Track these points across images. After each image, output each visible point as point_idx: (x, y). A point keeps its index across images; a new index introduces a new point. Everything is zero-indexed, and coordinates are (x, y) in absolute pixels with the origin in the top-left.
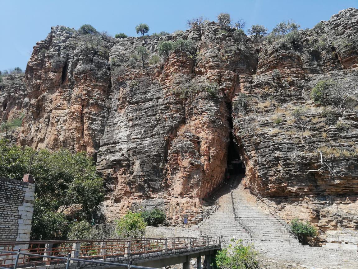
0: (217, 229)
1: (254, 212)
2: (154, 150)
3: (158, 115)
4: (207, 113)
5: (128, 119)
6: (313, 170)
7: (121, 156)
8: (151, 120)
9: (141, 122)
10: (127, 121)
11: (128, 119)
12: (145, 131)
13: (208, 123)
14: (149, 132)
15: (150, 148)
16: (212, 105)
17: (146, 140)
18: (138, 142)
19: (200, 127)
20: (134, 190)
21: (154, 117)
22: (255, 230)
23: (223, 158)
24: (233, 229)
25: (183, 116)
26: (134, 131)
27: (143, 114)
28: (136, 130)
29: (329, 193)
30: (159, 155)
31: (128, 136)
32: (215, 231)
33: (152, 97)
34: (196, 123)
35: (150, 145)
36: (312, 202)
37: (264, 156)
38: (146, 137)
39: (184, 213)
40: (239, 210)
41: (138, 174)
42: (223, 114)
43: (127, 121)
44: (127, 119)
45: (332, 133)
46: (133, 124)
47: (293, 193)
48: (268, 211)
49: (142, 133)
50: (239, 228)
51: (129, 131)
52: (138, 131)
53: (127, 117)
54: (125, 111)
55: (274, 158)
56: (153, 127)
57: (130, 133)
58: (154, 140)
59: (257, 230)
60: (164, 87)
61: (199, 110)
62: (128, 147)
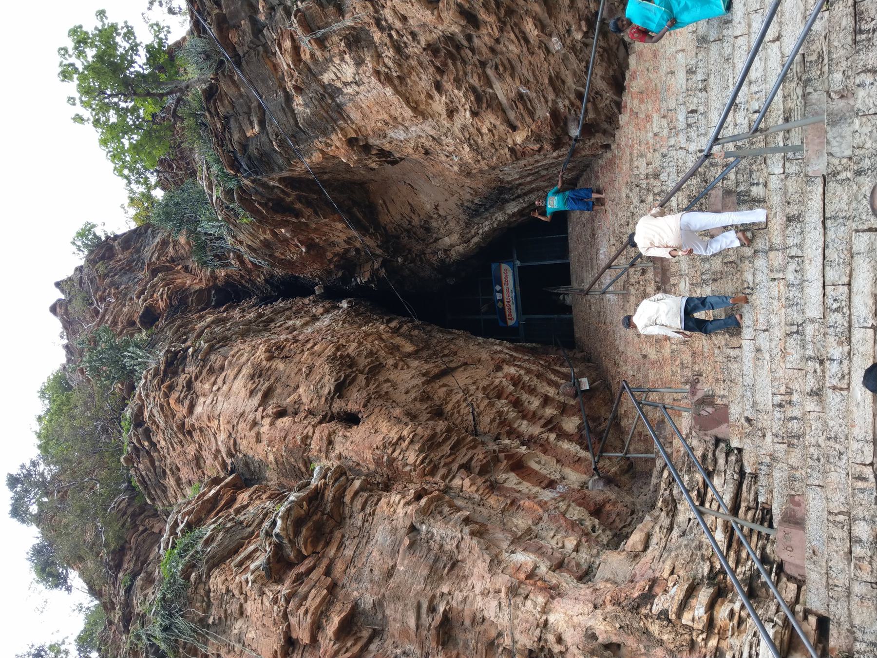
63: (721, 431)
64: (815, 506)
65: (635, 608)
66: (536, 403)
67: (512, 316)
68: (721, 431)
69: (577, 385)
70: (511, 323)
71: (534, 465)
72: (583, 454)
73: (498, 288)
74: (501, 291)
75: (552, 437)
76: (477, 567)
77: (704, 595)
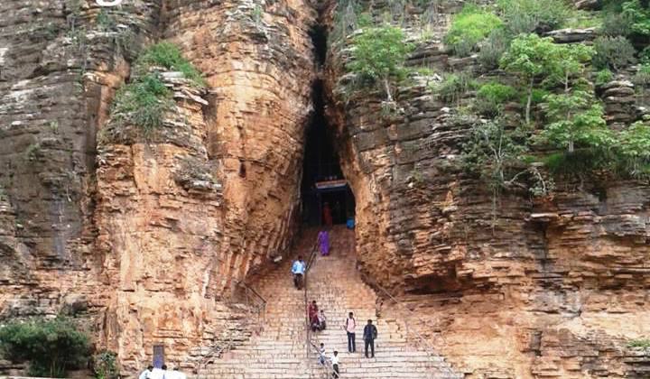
15: (30, 119)
17: (15, 86)
23: (290, 172)
29: (575, 280)
37: (411, 165)
38: (17, 78)
42: (294, 14)
45: (616, 99)
69: (276, 256)
70: (317, 184)
71: (237, 257)
72: (246, 273)
73: (336, 177)
74: (333, 180)
75: (250, 259)
77: (212, 337)
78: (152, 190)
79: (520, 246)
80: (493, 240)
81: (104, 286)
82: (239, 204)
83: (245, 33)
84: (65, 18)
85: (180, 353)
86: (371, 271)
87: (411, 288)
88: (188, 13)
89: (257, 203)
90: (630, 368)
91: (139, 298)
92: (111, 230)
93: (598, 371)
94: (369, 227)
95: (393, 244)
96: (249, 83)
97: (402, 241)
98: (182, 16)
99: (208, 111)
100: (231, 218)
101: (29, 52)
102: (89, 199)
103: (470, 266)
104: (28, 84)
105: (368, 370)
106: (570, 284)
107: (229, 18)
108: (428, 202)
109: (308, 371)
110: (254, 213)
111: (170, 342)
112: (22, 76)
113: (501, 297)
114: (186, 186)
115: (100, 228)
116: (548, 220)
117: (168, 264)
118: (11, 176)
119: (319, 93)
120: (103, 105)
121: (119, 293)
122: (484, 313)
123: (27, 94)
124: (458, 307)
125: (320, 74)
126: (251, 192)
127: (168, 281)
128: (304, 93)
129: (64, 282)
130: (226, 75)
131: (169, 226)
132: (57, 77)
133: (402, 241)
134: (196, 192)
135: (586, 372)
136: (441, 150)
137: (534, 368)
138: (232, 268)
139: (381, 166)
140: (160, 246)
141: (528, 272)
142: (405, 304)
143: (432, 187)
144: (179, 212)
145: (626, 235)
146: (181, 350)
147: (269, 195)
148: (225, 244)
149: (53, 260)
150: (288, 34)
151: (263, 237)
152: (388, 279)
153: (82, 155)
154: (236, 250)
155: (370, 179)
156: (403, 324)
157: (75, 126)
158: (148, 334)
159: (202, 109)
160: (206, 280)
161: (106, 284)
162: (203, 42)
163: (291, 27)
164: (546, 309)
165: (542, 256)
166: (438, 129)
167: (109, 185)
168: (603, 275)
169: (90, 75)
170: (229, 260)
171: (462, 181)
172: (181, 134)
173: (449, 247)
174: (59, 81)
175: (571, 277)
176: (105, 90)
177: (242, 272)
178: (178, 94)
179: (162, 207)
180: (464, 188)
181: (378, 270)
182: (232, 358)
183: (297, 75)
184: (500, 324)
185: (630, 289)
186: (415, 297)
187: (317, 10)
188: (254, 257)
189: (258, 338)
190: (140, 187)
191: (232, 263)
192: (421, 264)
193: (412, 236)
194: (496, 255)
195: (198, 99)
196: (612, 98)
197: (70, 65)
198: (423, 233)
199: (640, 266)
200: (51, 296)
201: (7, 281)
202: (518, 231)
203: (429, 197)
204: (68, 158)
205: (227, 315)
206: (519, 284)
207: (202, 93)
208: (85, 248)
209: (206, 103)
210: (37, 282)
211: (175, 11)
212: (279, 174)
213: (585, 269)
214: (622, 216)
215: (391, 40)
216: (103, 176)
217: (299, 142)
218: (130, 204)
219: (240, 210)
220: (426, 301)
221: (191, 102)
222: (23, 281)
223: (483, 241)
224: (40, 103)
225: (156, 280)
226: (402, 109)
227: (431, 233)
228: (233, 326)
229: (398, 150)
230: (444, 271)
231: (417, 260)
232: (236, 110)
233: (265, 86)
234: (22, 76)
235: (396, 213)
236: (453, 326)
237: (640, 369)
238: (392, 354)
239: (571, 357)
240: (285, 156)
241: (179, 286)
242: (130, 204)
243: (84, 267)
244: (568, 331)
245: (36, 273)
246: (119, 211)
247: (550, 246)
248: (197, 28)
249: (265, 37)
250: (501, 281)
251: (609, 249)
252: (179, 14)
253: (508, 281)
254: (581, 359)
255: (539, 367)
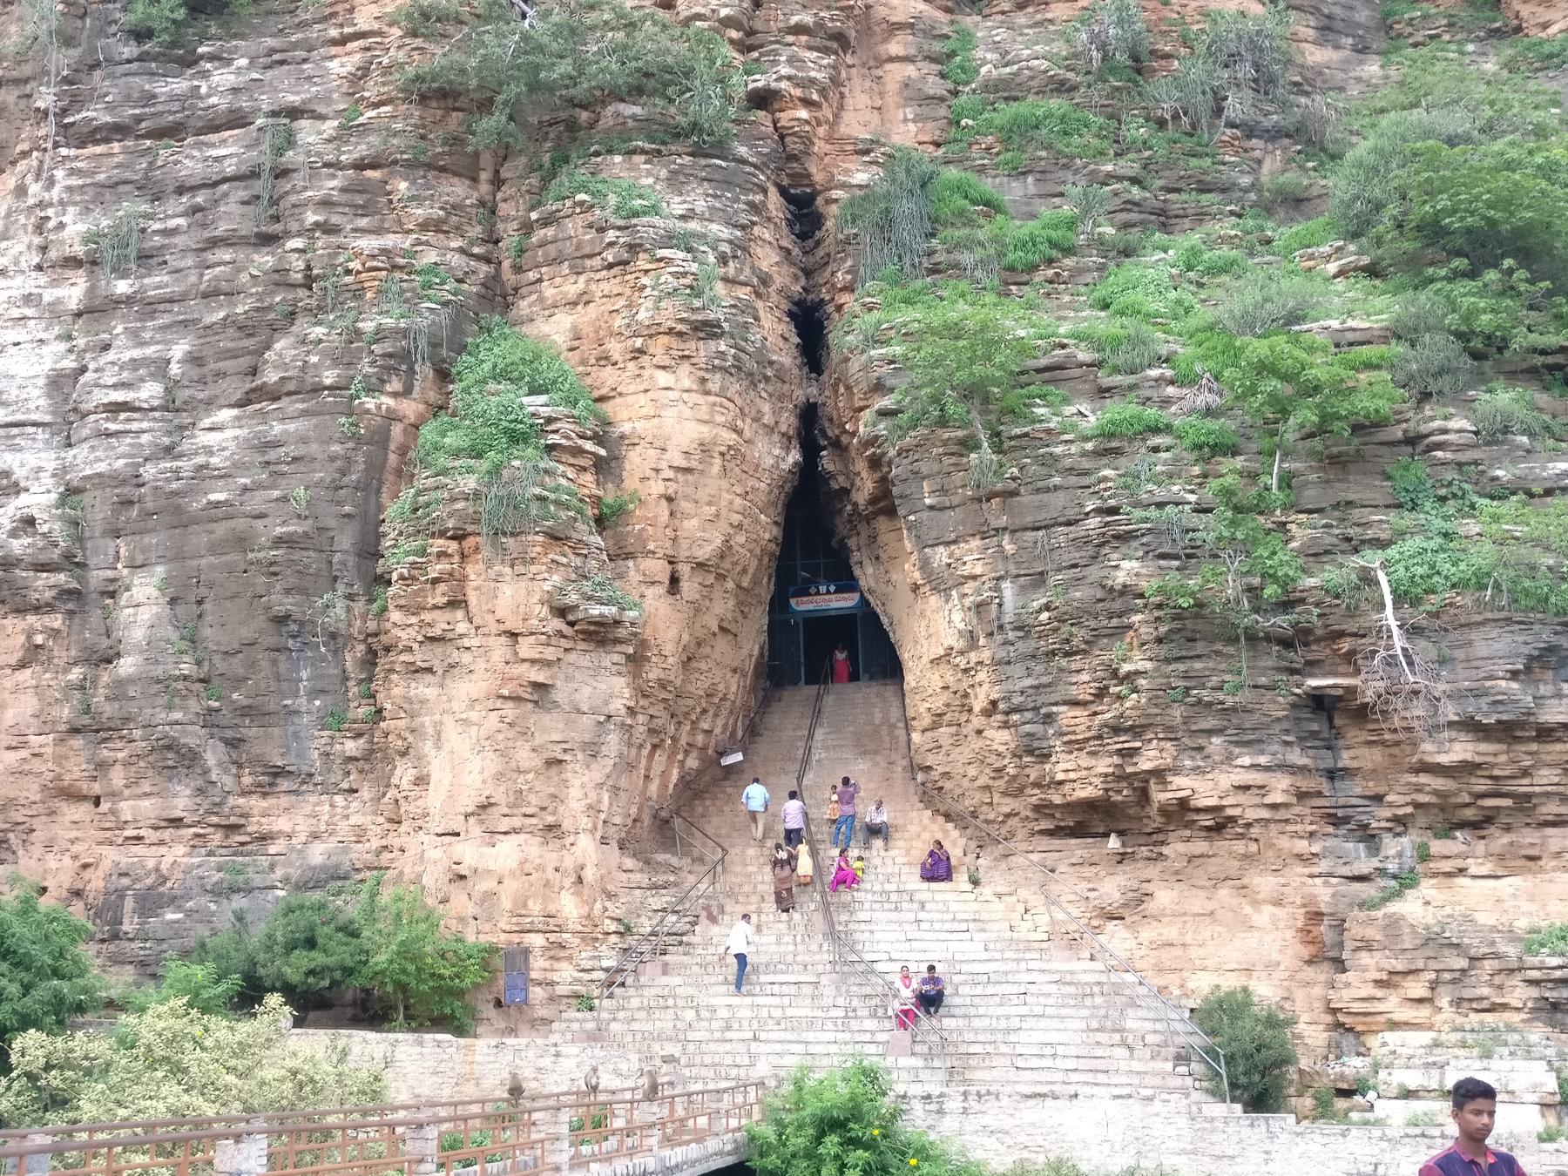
0: (728, 1035)
1: (956, 926)
2: (284, 499)
3: (298, 243)
4: (668, 261)
5: (53, 254)
6: (1331, 681)
7: (13, 534)
8: (244, 278)
9: (157, 282)
10: (39, 268)
11: (53, 254)
12: (194, 359)
13: (671, 331)
14: (235, 364)
15: (245, 489)
16: (701, 205)
17: (207, 423)
18: (145, 438)
19: (616, 357)
20: (117, 777)
21: (265, 260)
22: (971, 1037)
23: (756, 582)
24: (831, 1036)
25: (484, 268)
26: (106, 347)
27: (172, 223)
28: (122, 340)
29: (1400, 812)
30: (315, 540)
31: (60, 384)
32: (713, 1047)
33: (245, 103)
34: (587, 330)
35: (240, 466)
36: (1307, 871)
37: (1040, 579)
38: (210, 404)
39: (503, 937)
40: (861, 916)
41: (158, 671)
42: (765, 280)
43: (39, 268)
44: (44, 249)
45: (1449, 456)
46: (91, 291)
47: (1198, 810)
48: (1046, 918)
49: (175, 369)
50: (871, 1024)
51: (63, 346)
52: (137, 353)
53: (37, 240)
54: (21, 191)
55: (1100, 594)
56: (260, 330)
57: (69, 363)
58: (278, 428)
59: (981, 1038)
60: (334, 33)
61: (611, 235)
62: (64, 470)
63: (703, 919)
64: (674, 980)
65: (604, 891)
66: (706, 726)
67: (802, 605)
68: (703, 919)
70: (793, 602)
72: (671, 786)
73: (832, 588)
74: (828, 592)
76: (598, 772)
78: (502, 627)
79: (1287, 743)
80: (1229, 732)
81: (387, 826)
82: (668, 648)
83: (682, 320)
84: (310, 289)
85: (556, 965)
86: (948, 785)
87: (1046, 824)
88: (558, 280)
89: (699, 645)
90: (1534, 992)
91: (469, 852)
92: (411, 709)
93: (1471, 1000)
94: (945, 697)
95: (1006, 732)
96: (688, 413)
97: (1027, 728)
98: (546, 283)
99: (606, 467)
100: (651, 676)
101: (234, 355)
102: (361, 647)
103: (1182, 785)
104: (237, 418)
105: (977, 1000)
106: (1388, 820)
107: (648, 291)
108: (1085, 652)
109: (840, 1001)
110: (694, 664)
111: (537, 940)
112: (222, 401)
113: (1253, 847)
114: (571, 618)
115: (388, 706)
116: (1340, 692)
117: (531, 776)
118: (200, 603)
119: (810, 429)
120: (393, 458)
121: (426, 839)
122: (1218, 881)
123: (237, 438)
124: (1160, 866)
125: (813, 390)
126: (690, 625)
127: (529, 811)
128: (784, 429)
129: (300, 820)
130: (642, 399)
131: (535, 697)
132: (300, 406)
133: (1027, 728)
134: (592, 628)
135: (1444, 1002)
136: (1106, 550)
137: (1332, 995)
138: (647, 777)
139: (974, 577)
140: (515, 740)
141: (1302, 796)
142: (1035, 857)
143: (1093, 624)
144: (555, 669)
145: (1499, 722)
146: (558, 959)
147: (721, 628)
148: (640, 731)
149: (278, 773)
150: (757, 319)
151: (704, 711)
152: (991, 804)
153: (352, 561)
154: (656, 741)
155: (947, 601)
156: (1037, 901)
157: (338, 503)
158: (487, 927)
159: (595, 465)
160: (605, 805)
161: (391, 821)
162: (592, 335)
163: (759, 304)
164: (1346, 871)
165: (1329, 763)
166: (1099, 511)
167: (414, 620)
168: (1453, 800)
169: (370, 403)
170: (644, 762)
171: (1157, 613)
172: (563, 514)
173: (1138, 744)
174: (304, 414)
175: (1391, 805)
176: (397, 430)
177: (664, 786)
178: (554, 439)
179: (524, 660)
180: (1163, 629)
181: (965, 783)
182: (665, 973)
183: (771, 395)
184: (1256, 903)
185: (1508, 829)
186: (1056, 843)
187: (802, 270)
188: (687, 753)
189: (715, 929)
190: (477, 621)
191: (648, 769)
192: (1072, 775)
193: (1049, 719)
194: (1239, 762)
195: (589, 446)
196: (1439, 454)
197: (328, 382)
198: (1078, 713)
199: (1526, 781)
200: (272, 850)
201: (181, 819)
202: (1281, 714)
203: (1086, 642)
204: (324, 566)
205: (645, 882)
206: (1287, 821)
207: (596, 433)
208: (351, 747)
209: (603, 452)
210: (242, 821)
211: (532, 275)
212: (739, 587)
213: (1419, 789)
214: (1488, 684)
215: (987, 341)
216: (402, 602)
217: (776, 523)
218: (456, 656)
219: (671, 660)
220: (1085, 853)
221: (580, 451)
222: (214, 819)
223: (1210, 732)
224: (266, 458)
225: (506, 811)
226: (1015, 470)
227: (1095, 714)
228: (657, 902)
229: (1009, 548)
230: (1125, 792)
231: (1063, 765)
232: (663, 465)
233: (720, 419)
234: (222, 401)
235: (1017, 670)
236: (1151, 906)
237: (1555, 994)
238: (1023, 965)
239: (1410, 972)
240: (751, 551)
241: (550, 819)
242: (456, 656)
243: (345, 785)
244: (1403, 918)
245: (241, 801)
246: (430, 670)
247: (1341, 743)
248: (579, 307)
249: (720, 327)
250: (1251, 814)
251: (1461, 750)
252: (540, 280)
253: (1265, 814)
254: (1433, 976)
255: (1347, 994)
